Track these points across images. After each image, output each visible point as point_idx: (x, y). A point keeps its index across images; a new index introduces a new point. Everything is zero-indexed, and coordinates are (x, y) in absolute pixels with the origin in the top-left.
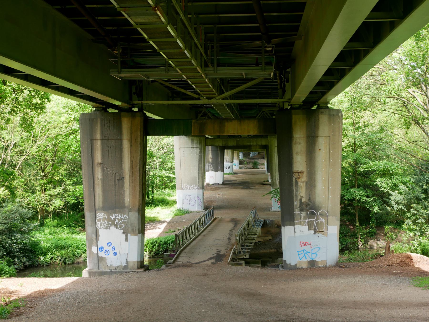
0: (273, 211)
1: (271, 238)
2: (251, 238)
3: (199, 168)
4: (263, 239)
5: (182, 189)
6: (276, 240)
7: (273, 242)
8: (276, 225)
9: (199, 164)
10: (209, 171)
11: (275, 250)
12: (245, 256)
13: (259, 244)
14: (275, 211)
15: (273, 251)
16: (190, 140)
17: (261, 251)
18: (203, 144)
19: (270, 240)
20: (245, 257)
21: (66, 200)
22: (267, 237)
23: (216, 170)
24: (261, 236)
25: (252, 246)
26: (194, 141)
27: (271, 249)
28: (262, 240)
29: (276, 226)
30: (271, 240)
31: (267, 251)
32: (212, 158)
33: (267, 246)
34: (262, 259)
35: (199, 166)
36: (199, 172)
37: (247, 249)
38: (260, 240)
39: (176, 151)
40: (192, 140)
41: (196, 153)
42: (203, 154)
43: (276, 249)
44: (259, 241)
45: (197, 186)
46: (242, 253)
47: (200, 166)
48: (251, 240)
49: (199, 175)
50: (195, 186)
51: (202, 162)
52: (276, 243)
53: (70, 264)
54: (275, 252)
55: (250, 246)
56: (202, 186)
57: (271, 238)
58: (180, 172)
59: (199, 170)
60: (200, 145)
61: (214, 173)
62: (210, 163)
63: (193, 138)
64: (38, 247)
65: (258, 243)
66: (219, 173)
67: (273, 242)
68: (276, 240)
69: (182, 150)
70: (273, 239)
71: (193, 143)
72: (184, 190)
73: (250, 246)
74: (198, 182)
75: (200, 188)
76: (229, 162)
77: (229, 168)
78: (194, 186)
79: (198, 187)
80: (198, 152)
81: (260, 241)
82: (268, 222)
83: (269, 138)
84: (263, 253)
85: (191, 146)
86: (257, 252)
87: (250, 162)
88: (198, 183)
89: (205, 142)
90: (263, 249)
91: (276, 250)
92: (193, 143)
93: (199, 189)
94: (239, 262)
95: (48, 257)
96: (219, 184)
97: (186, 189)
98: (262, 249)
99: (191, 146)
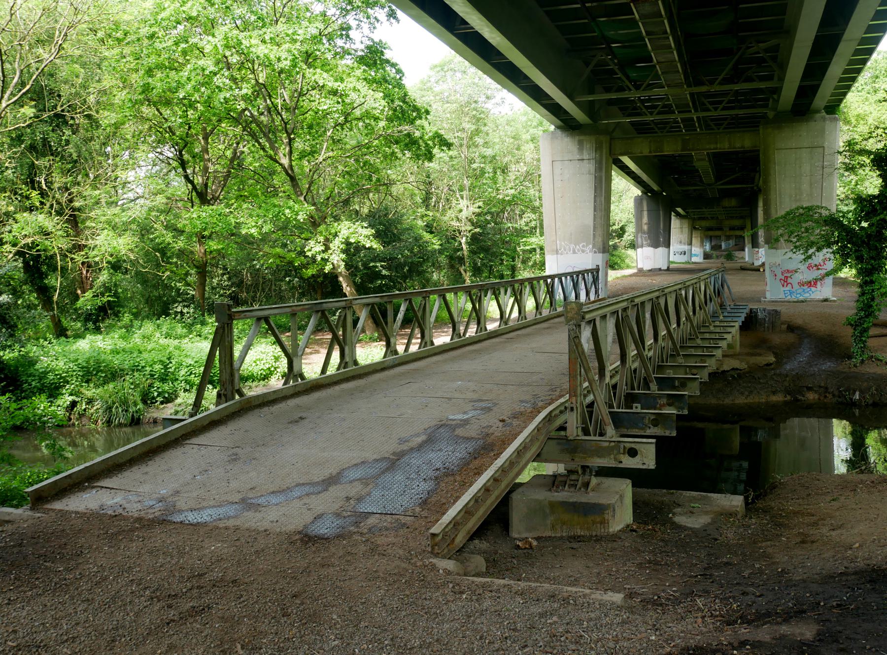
0: (769, 302)
1: (772, 359)
2: (700, 350)
3: (595, 206)
4: (747, 363)
5: (557, 252)
6: (788, 367)
7: (778, 371)
8: (785, 324)
9: (595, 196)
10: (642, 247)
11: (785, 397)
12: (633, 453)
13: (733, 377)
14: (773, 301)
15: (778, 398)
16: (576, 143)
17: (741, 400)
18: (604, 151)
19: (767, 365)
20: (629, 463)
21: (84, 228)
22: (760, 355)
23: (655, 245)
24: (739, 354)
25: (696, 385)
26: (585, 143)
27: (774, 393)
28: (743, 366)
29: (784, 327)
30: (772, 366)
31: (759, 398)
32: (648, 224)
33: (760, 383)
34: (742, 423)
35: (595, 201)
36: (594, 215)
37: (664, 401)
38: (735, 363)
39: (545, 169)
40: (581, 144)
41: (590, 171)
42: (604, 174)
43: (788, 392)
44: (733, 369)
45: (591, 246)
46: (610, 431)
47: (598, 200)
48: (699, 359)
49: (594, 220)
50: (587, 245)
51: (602, 188)
52: (787, 376)
53: (126, 425)
54: (786, 403)
55: (683, 383)
56: (601, 247)
57: (772, 359)
58: (553, 215)
59: (595, 210)
60: (598, 151)
61: (651, 249)
62: (644, 233)
63: (582, 138)
64: (32, 370)
65: (733, 373)
66: (661, 250)
67: (778, 371)
68: (788, 367)
69: (558, 165)
70: (779, 363)
71: (583, 149)
72: (562, 254)
73: (683, 383)
74: (592, 236)
75: (599, 249)
76: (685, 244)
77: (685, 254)
78: (583, 246)
79: (593, 247)
80: (593, 170)
81: (737, 369)
82: (760, 315)
83: (761, 131)
84: (746, 404)
85: (578, 157)
86: (728, 401)
87: (721, 256)
88: (594, 239)
89: (610, 145)
90: (747, 393)
91: (789, 397)
92: (581, 149)
93: (595, 252)
94: (591, 497)
95: (60, 402)
96: (660, 269)
97: (567, 253)
98: (742, 394)
99: (578, 157)
